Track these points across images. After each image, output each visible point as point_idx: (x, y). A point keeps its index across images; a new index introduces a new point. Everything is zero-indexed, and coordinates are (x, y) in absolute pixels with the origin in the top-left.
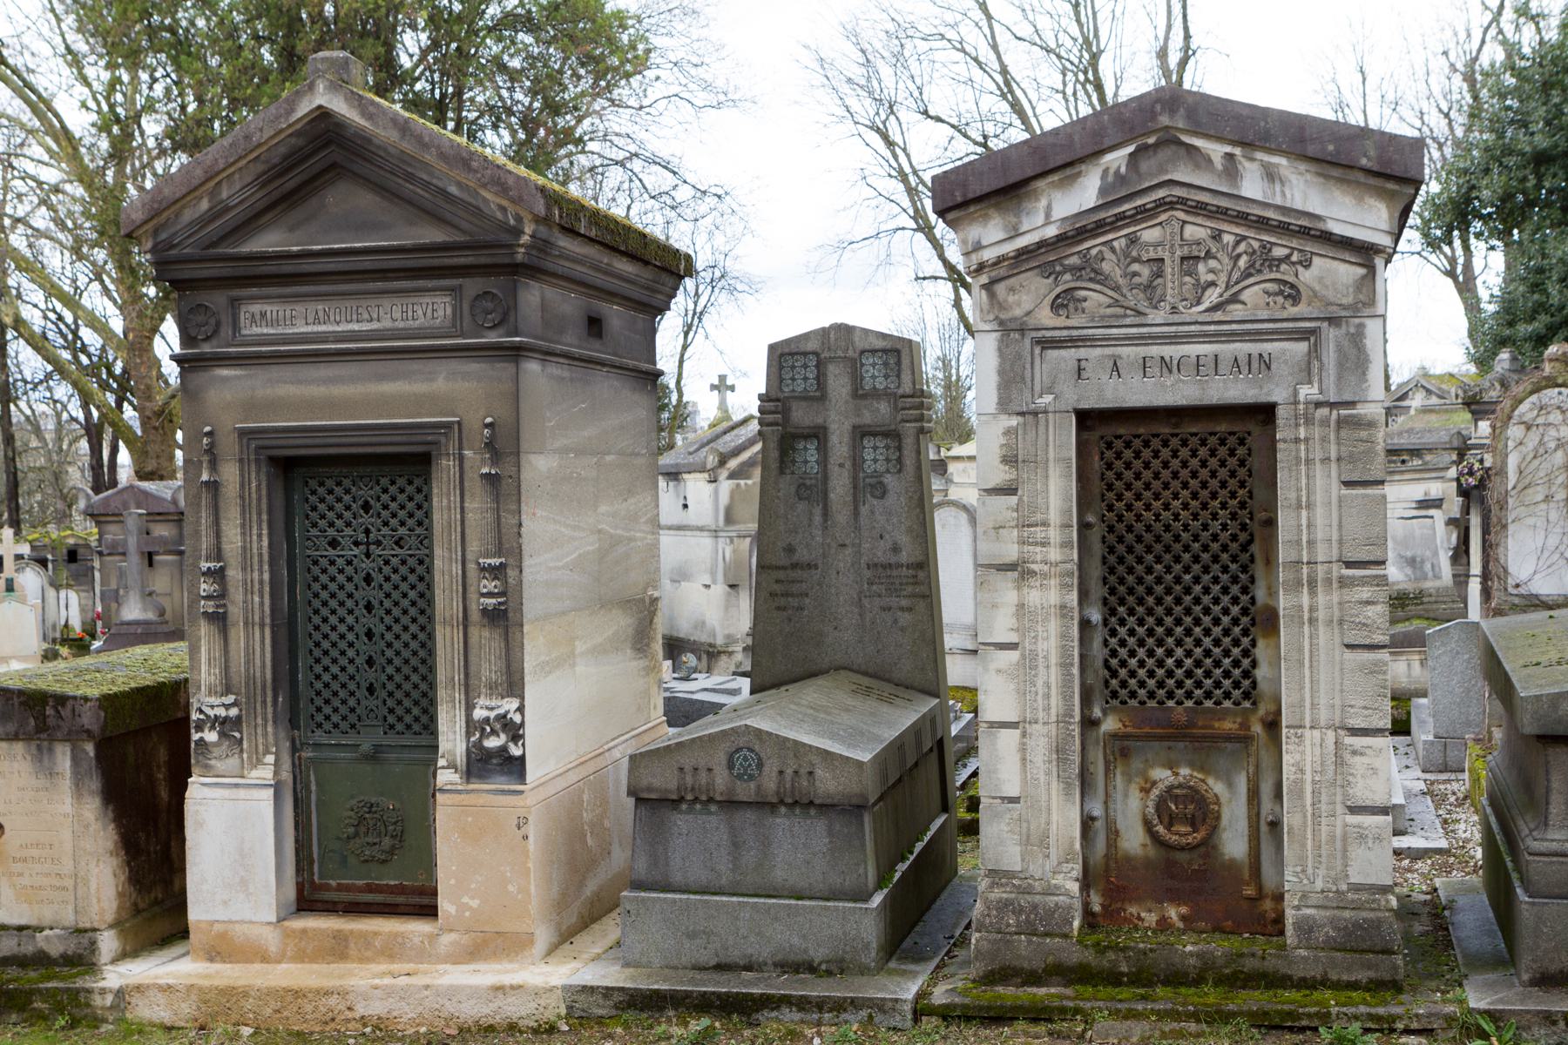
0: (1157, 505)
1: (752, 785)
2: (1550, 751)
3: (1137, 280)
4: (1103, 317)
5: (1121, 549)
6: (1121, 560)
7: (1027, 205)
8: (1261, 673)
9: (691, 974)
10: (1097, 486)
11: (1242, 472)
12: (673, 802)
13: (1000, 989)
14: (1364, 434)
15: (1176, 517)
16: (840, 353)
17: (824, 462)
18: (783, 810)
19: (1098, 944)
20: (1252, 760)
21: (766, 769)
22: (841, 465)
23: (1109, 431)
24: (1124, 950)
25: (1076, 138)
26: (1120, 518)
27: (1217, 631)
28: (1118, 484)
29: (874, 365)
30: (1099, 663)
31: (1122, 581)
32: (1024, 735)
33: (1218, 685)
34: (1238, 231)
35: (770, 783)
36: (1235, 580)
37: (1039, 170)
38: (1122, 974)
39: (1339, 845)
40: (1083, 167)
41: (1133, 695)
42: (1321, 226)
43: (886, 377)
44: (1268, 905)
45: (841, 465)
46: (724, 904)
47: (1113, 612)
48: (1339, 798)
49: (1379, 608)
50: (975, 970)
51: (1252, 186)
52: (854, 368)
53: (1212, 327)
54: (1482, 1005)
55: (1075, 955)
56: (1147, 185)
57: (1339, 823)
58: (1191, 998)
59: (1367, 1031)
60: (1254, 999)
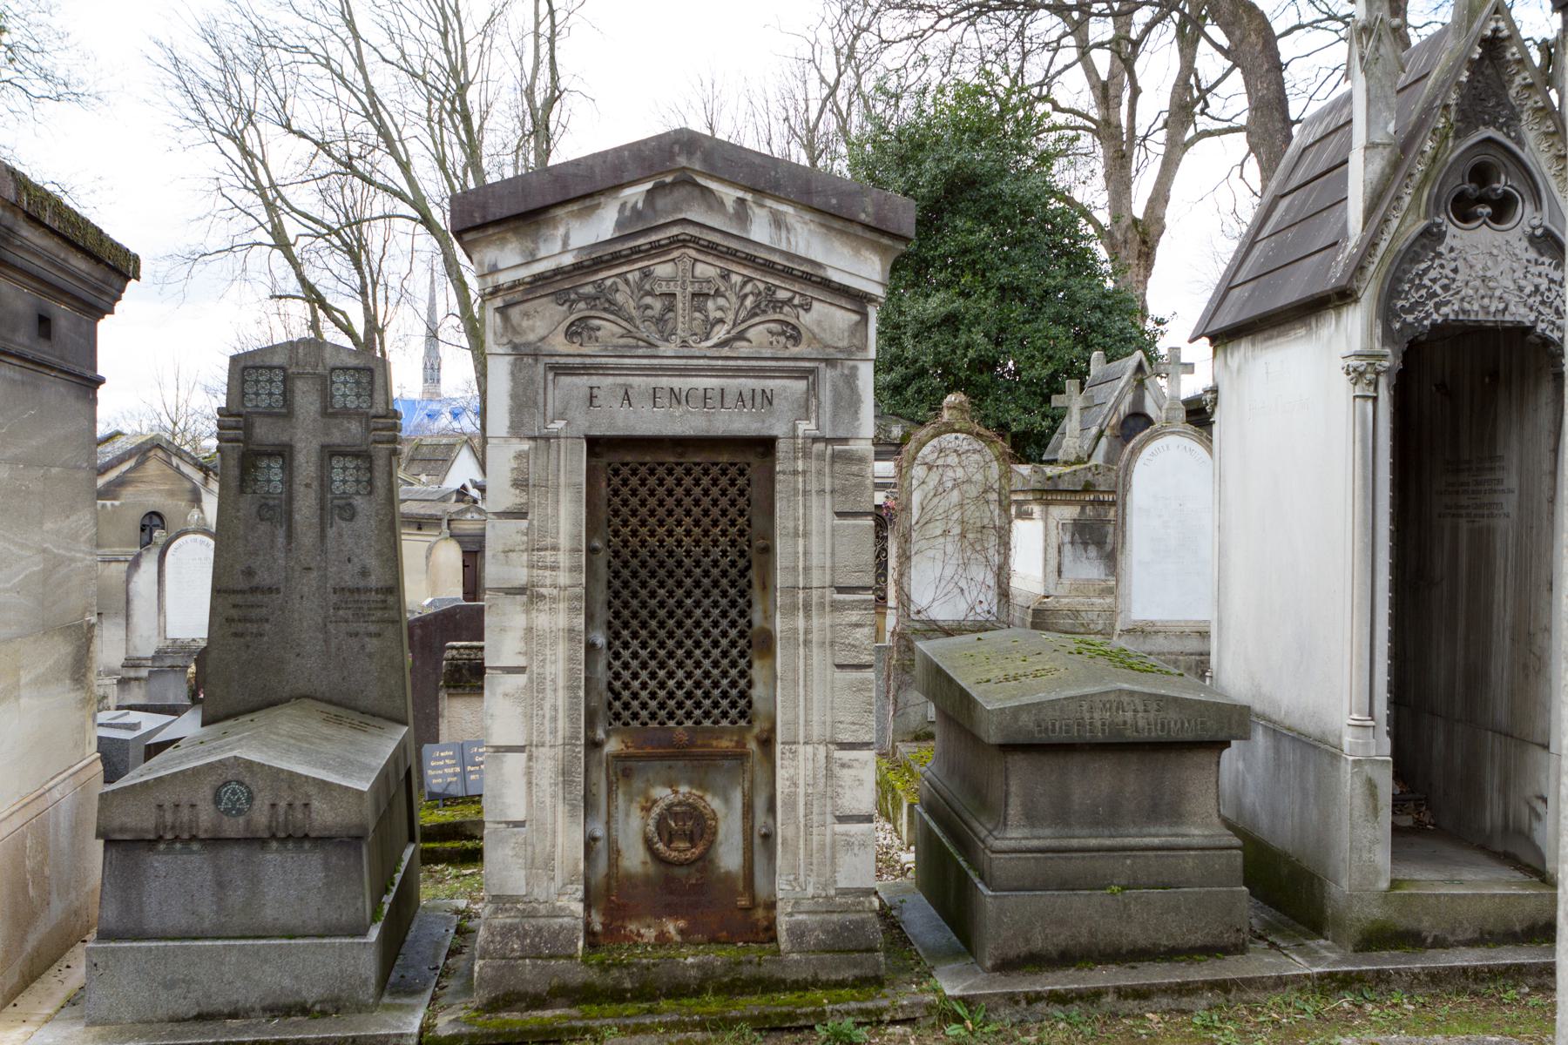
0: (661, 531)
1: (241, 820)
2: (1009, 758)
3: (649, 312)
4: (616, 347)
5: (626, 573)
6: (626, 584)
7: (545, 232)
8: (757, 693)
9: (169, 1027)
10: (604, 512)
11: (742, 502)
12: (149, 843)
13: (504, 1015)
14: (855, 469)
15: (679, 543)
16: (309, 369)
17: (289, 481)
18: (274, 845)
19: (603, 963)
20: (748, 776)
21: (257, 803)
22: (308, 486)
23: (616, 458)
24: (628, 966)
25: (597, 170)
26: (625, 543)
27: (716, 653)
28: (624, 510)
29: (345, 383)
30: (603, 686)
31: (626, 605)
32: (530, 758)
33: (716, 705)
34: (745, 272)
35: (260, 817)
36: (733, 604)
37: (560, 199)
38: (626, 990)
39: (828, 853)
40: (602, 199)
41: (635, 716)
42: (821, 273)
43: (358, 396)
44: (760, 913)
45: (308, 486)
46: (207, 949)
47: (617, 635)
48: (829, 809)
49: (866, 630)
50: (479, 997)
51: (760, 231)
52: (324, 385)
53: (720, 362)
54: (957, 992)
55: (579, 974)
56: (662, 221)
57: (828, 832)
58: (695, 1008)
59: (859, 1024)
60: (752, 1004)
